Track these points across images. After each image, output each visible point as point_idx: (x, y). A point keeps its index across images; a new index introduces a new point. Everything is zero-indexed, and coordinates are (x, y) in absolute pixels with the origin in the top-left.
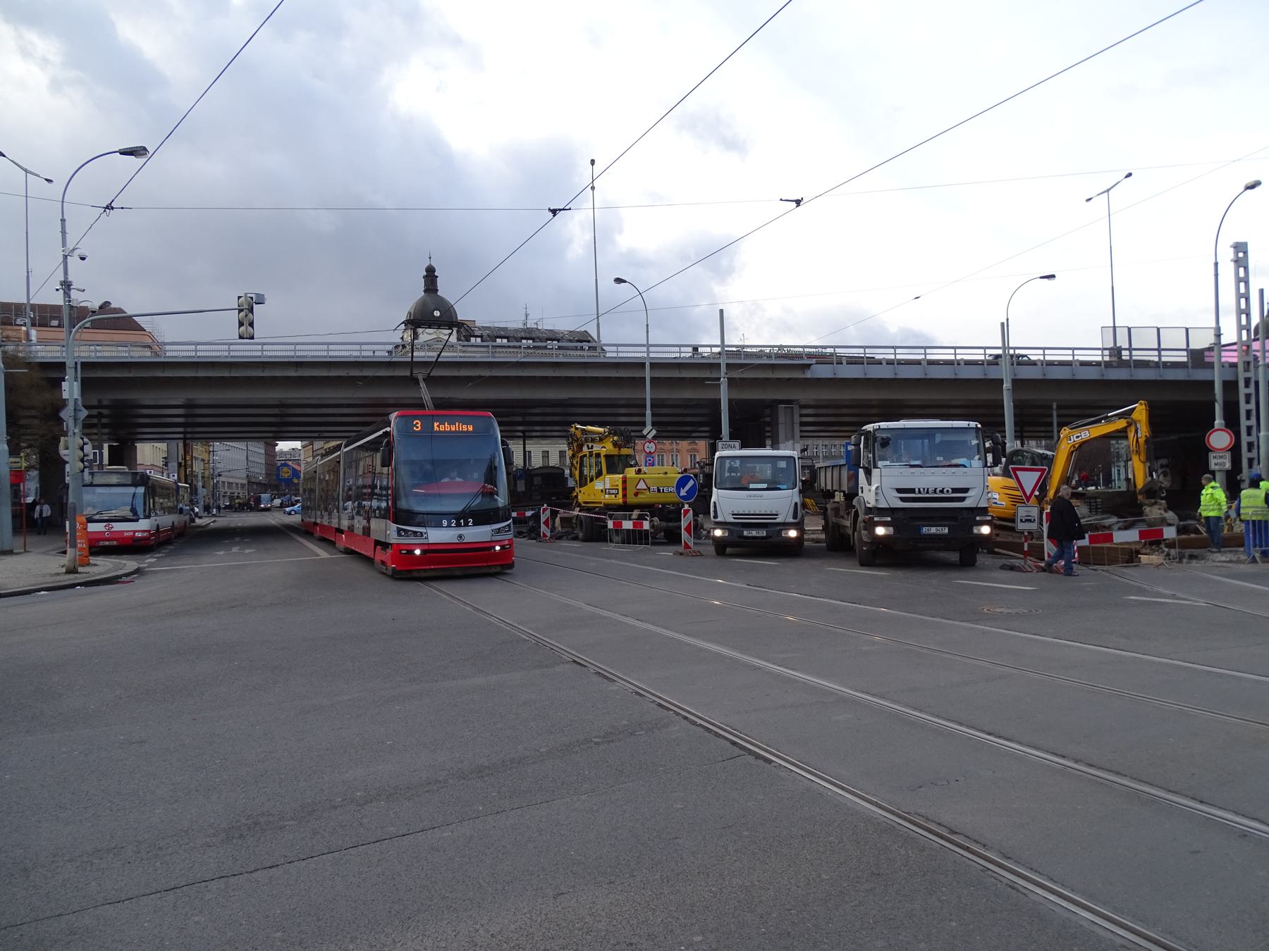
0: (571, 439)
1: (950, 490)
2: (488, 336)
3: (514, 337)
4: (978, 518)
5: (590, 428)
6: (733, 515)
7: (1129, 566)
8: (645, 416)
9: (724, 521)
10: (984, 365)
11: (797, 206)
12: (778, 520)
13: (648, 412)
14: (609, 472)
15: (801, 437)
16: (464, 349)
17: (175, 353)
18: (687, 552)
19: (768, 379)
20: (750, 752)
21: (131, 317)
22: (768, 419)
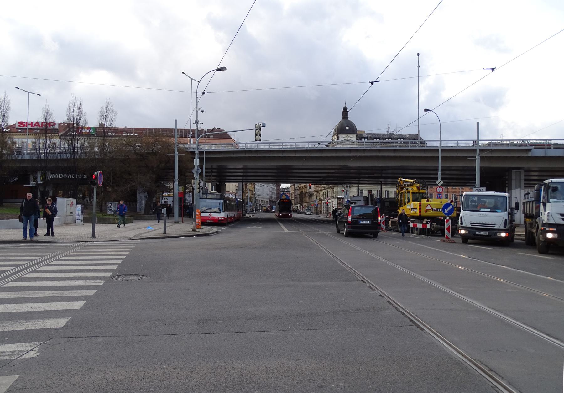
0: (398, 185)
2: (371, 137)
3: (382, 138)
5: (407, 180)
6: (471, 223)
8: (438, 175)
9: (466, 226)
11: (492, 71)
12: (495, 228)
13: (440, 173)
14: (414, 201)
15: (525, 187)
16: (359, 144)
17: (241, 147)
18: (447, 240)
19: (506, 157)
20: (416, 325)
21: (226, 132)
22: (507, 177)
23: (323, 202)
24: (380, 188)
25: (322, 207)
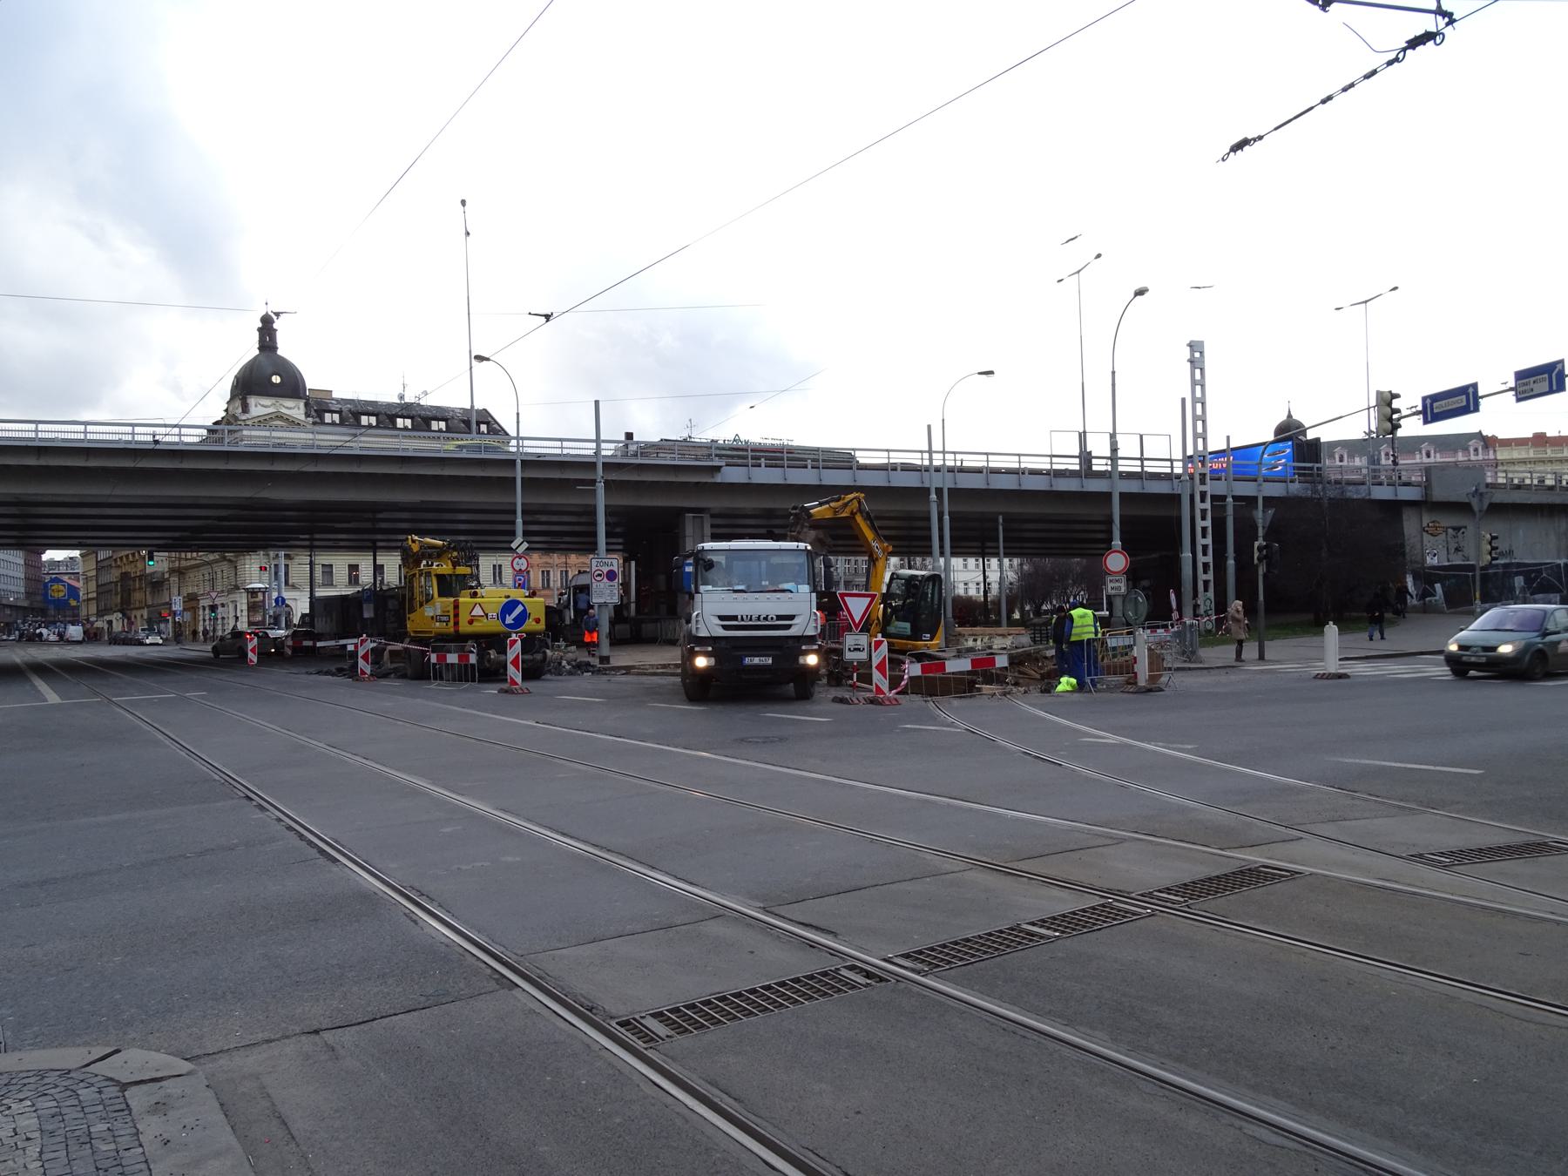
1: (775, 617)
4: (804, 647)
7: (964, 697)
13: (519, 521)
23: (202, 603)
24: (372, 557)
25: (201, 618)
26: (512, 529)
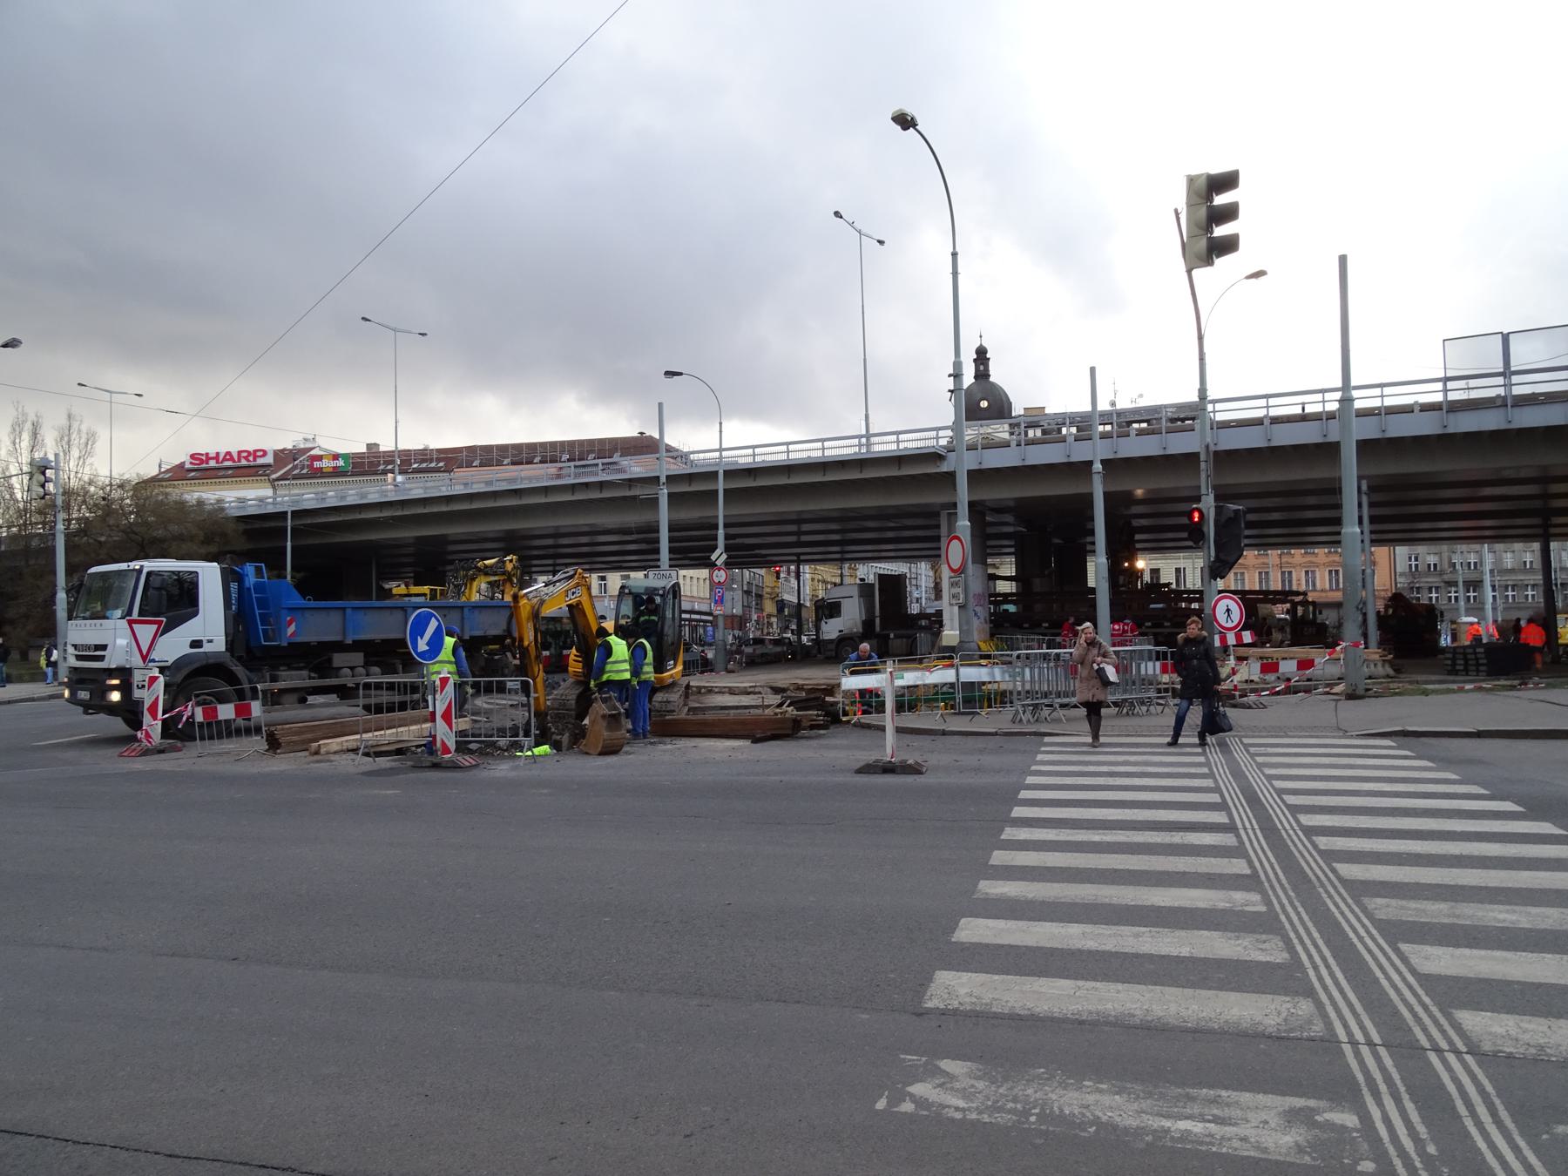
10: (1380, 415)
13: (721, 532)
26: (937, 534)
